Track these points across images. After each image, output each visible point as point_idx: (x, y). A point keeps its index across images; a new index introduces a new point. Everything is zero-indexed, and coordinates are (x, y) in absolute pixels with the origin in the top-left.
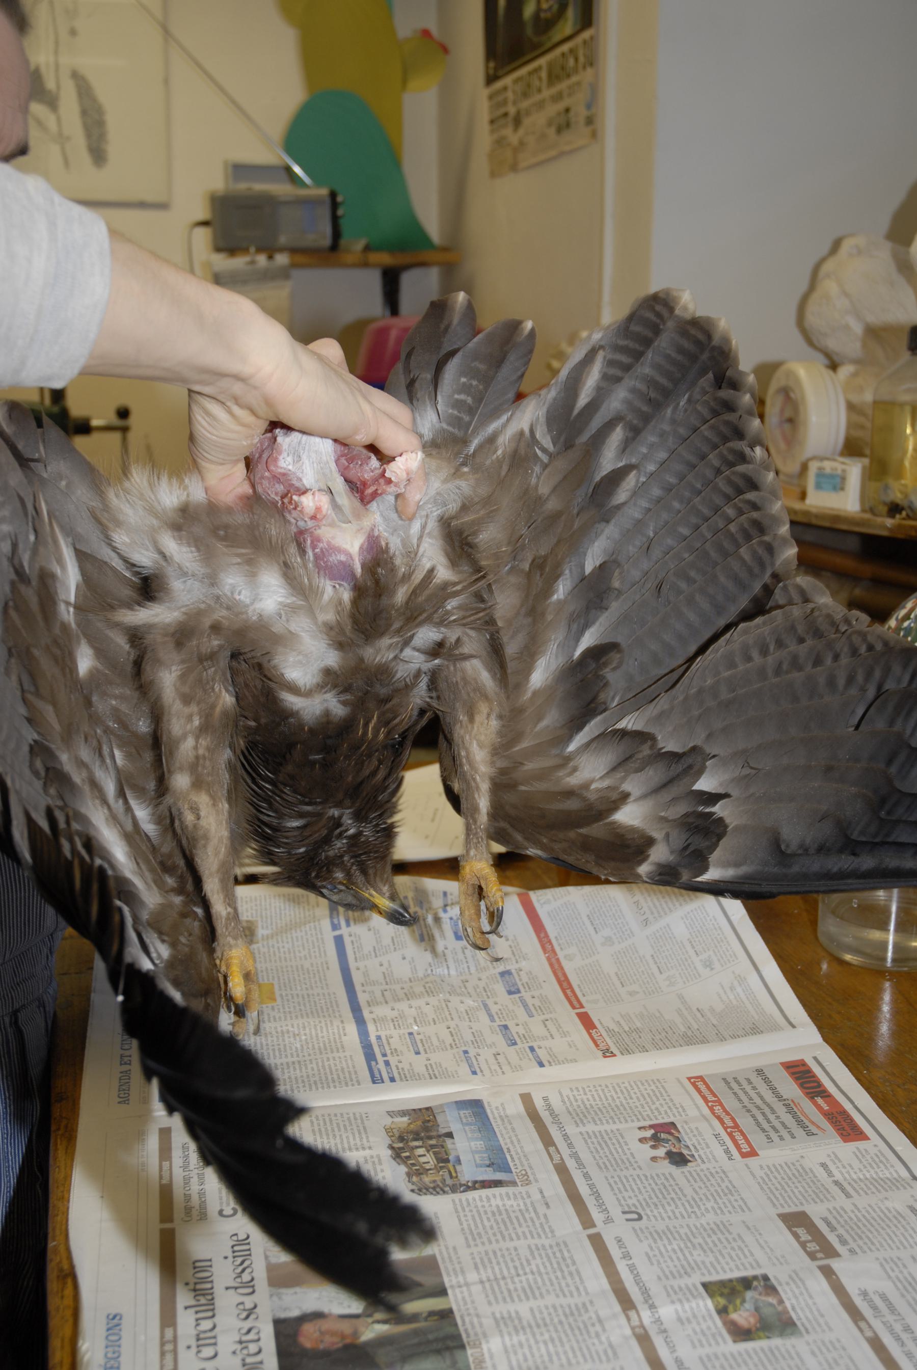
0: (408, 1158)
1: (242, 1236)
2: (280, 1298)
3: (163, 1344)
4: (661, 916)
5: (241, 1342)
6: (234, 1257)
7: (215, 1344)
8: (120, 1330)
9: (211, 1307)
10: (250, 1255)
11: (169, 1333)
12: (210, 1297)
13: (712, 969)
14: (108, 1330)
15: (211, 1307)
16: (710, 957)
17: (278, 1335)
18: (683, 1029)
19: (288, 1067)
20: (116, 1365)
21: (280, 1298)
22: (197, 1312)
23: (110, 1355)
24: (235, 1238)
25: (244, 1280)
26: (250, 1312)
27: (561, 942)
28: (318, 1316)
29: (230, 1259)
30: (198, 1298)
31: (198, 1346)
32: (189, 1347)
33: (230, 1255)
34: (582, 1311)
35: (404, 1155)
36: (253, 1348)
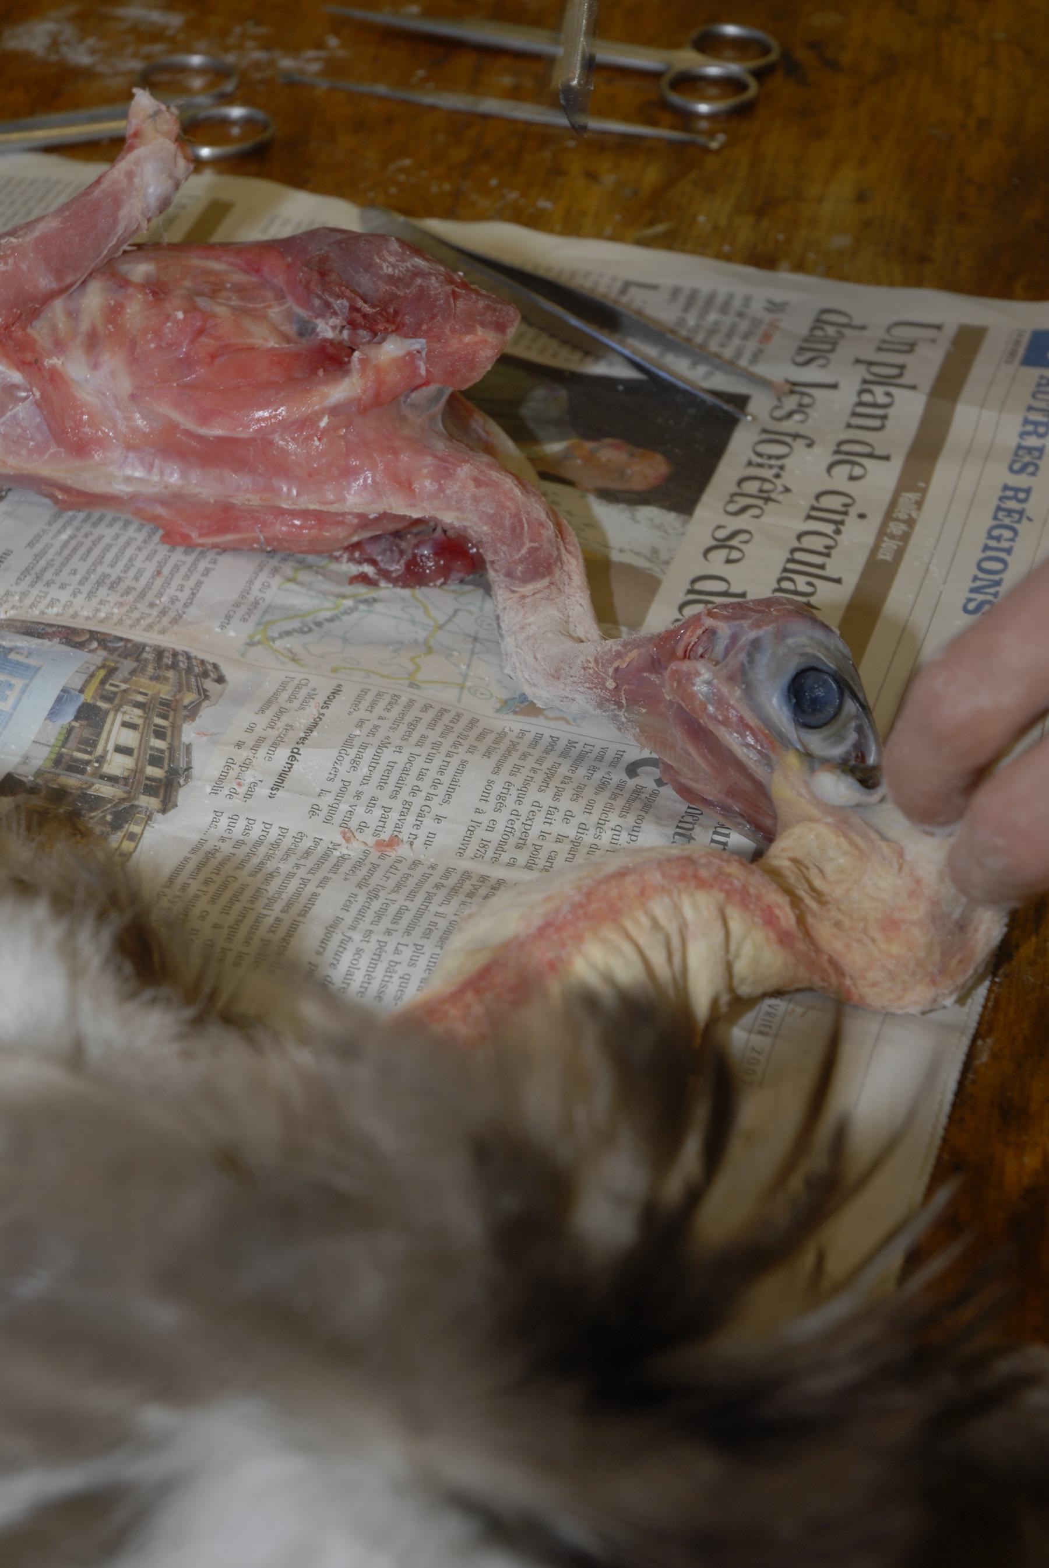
0: (155, 760)
3: (905, 537)
8: (975, 578)
11: (886, 554)
20: (1000, 515)
21: (655, 551)
22: (822, 567)
26: (722, 544)
30: (809, 589)
31: (846, 513)
32: (862, 516)
36: (752, 487)
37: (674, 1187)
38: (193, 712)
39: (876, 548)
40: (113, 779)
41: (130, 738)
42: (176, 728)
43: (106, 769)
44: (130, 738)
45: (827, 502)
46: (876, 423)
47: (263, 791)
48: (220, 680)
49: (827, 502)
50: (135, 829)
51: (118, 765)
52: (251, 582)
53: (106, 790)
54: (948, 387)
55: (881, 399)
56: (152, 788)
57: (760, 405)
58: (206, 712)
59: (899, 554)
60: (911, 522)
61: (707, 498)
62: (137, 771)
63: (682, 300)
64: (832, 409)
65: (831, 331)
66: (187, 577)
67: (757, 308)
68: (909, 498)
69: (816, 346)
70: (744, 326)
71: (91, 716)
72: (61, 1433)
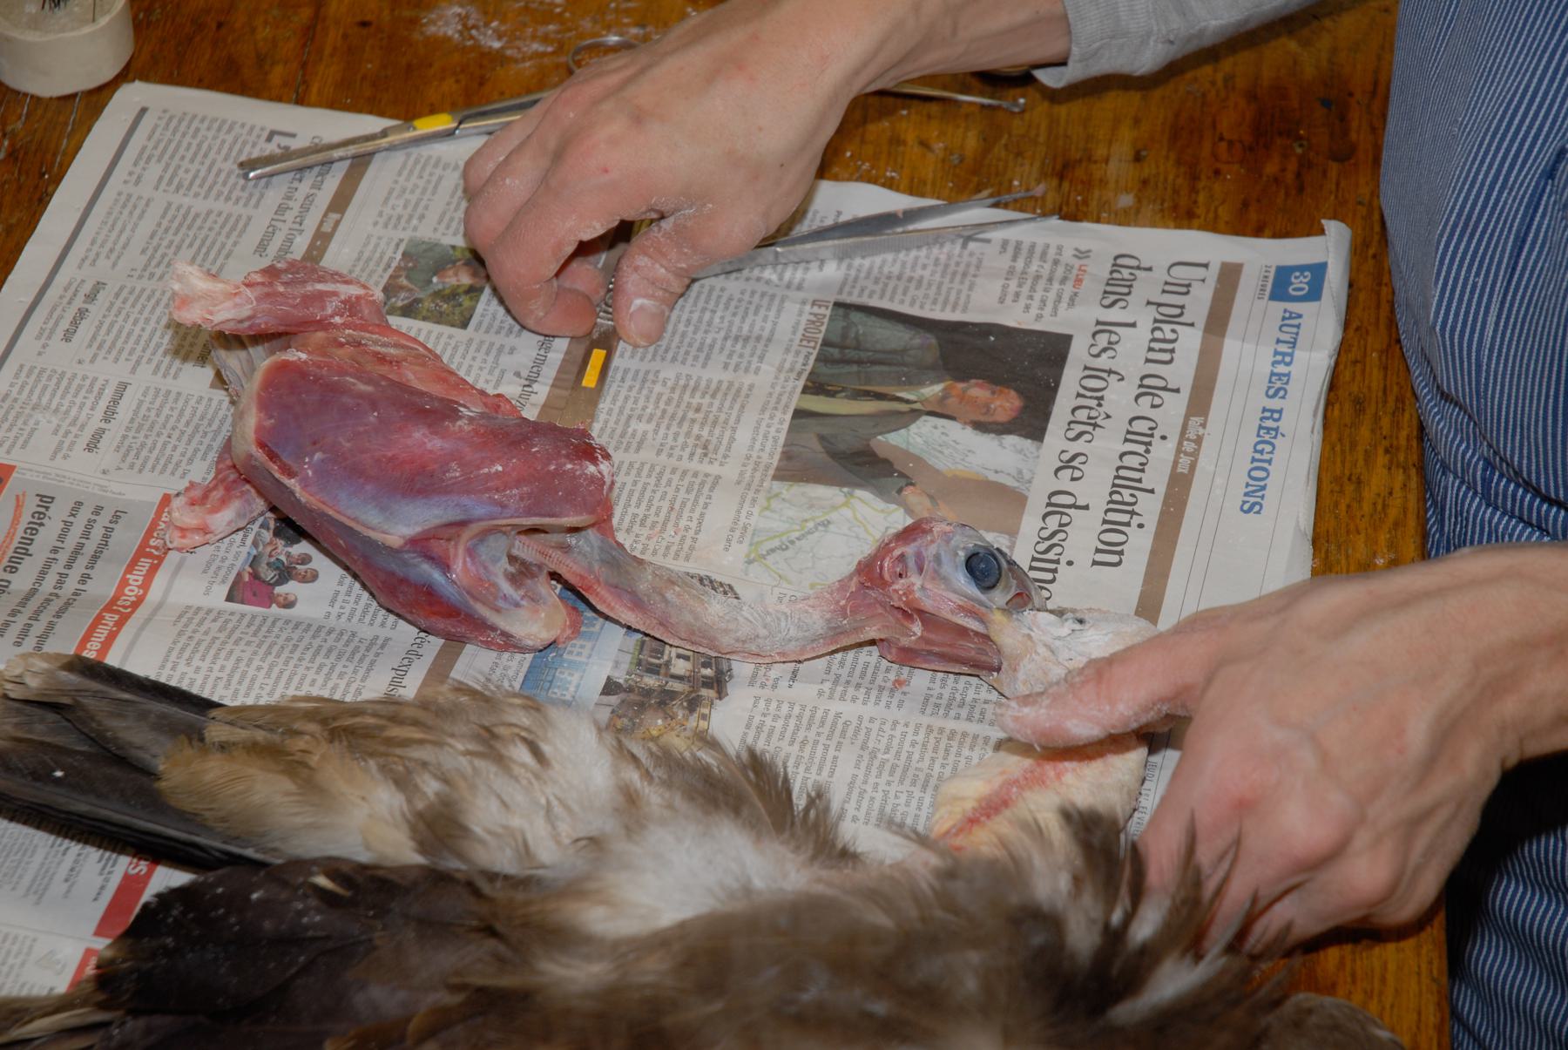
2: (1020, 472)
5: (1095, 425)
6: (1058, 562)
7: (1129, 432)
9: (1118, 482)
10: (1034, 559)
12: (1116, 497)
14: (1263, 488)
15: (1118, 482)
17: (1046, 416)
22: (1140, 481)
23: (1268, 448)
25: (1106, 335)
26: (1067, 465)
28: (981, 427)
29: (1063, 560)
32: (1164, 438)
33: (1062, 568)
34: (641, 375)
35: (708, 672)
36: (1082, 415)
37: (1117, 917)
39: (1176, 463)
40: (680, 678)
43: (673, 670)
46: (1166, 357)
50: (705, 711)
52: (739, 512)
53: (676, 686)
54: (1217, 323)
55: (1172, 336)
56: (708, 683)
57: (1078, 353)
59: (1193, 467)
60: (1199, 441)
63: (1010, 250)
65: (1126, 273)
66: (692, 511)
67: (1068, 255)
68: (1195, 421)
69: (1117, 288)
70: (1060, 271)
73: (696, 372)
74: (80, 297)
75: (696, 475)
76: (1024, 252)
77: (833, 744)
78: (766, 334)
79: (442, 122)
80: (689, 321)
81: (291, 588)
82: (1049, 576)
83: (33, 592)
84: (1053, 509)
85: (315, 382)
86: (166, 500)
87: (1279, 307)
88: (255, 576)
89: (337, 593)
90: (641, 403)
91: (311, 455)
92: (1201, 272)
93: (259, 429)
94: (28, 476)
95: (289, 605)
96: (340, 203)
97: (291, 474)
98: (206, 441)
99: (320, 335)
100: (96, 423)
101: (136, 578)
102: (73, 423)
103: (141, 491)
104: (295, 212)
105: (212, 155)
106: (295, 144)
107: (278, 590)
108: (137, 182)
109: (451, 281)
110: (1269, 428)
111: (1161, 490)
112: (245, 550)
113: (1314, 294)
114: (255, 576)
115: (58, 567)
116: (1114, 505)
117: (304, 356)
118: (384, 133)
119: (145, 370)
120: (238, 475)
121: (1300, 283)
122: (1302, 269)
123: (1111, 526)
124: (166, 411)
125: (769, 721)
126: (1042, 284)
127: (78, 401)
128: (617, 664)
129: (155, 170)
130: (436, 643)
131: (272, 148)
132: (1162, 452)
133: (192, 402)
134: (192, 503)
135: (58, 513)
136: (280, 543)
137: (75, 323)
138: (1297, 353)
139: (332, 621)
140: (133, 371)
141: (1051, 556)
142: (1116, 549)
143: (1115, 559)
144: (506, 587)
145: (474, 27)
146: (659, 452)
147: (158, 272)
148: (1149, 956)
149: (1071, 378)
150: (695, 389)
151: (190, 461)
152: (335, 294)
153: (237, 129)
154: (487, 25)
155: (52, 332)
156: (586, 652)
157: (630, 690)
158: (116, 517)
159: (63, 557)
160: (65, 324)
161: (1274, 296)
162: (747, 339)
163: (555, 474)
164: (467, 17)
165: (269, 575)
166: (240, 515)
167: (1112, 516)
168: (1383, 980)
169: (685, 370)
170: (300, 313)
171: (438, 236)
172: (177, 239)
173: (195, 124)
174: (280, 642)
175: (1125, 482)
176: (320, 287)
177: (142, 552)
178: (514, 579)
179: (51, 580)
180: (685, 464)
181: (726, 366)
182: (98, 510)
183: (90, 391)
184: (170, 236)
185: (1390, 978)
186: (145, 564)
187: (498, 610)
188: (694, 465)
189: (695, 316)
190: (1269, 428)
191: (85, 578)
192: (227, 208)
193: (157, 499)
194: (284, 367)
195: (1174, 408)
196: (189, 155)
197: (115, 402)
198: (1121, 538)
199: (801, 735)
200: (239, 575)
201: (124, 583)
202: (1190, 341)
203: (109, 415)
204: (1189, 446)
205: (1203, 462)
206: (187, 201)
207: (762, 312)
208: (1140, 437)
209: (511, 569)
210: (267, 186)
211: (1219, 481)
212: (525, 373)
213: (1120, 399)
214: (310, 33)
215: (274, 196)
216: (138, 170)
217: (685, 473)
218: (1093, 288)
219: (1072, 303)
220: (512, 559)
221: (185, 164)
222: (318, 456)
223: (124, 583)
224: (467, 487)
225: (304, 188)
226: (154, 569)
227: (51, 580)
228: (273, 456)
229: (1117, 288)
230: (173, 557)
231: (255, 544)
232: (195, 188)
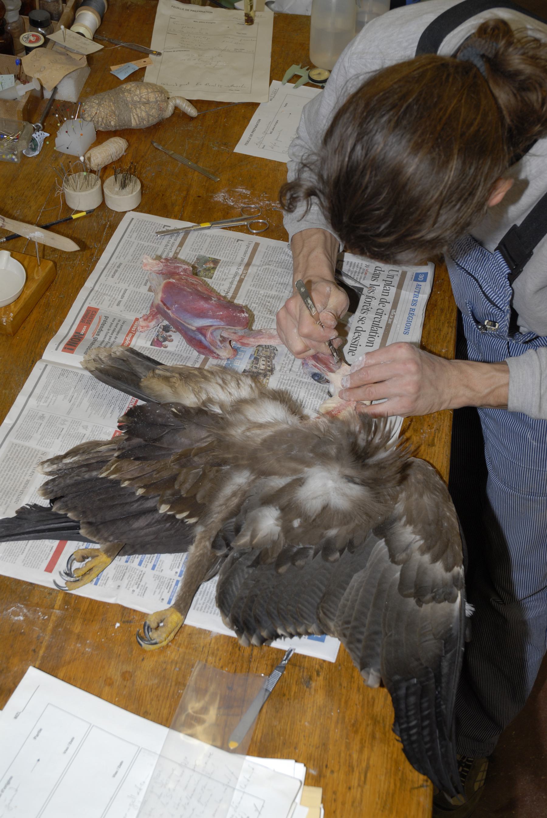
0: (269, 366)
1: (351, 353)
4: (36, 450)
13: (43, 415)
16: (38, 420)
18: (90, 392)
19: (297, 382)
24: (354, 354)
26: (361, 320)
27: (49, 551)
33: (358, 347)
35: (270, 368)
36: (365, 308)
37: (370, 438)
38: (274, 358)
39: (388, 321)
40: (262, 370)
41: (264, 363)
42: (271, 361)
44: (264, 363)
45: (379, 311)
46: (387, 294)
47: (288, 372)
48: (277, 350)
49: (379, 311)
51: (262, 367)
53: (261, 371)
54: (400, 286)
55: (388, 289)
56: (269, 371)
57: (365, 291)
58: (276, 358)
59: (392, 322)
60: (394, 316)
61: (357, 310)
62: (266, 368)
63: (349, 264)
64: (379, 290)
65: (378, 272)
67: (364, 266)
68: (393, 310)
69: (375, 276)
70: (361, 270)
71: (257, 359)
72: (295, 471)
73: (269, 292)
74: (116, 267)
75: (268, 318)
76: (353, 265)
77: (299, 387)
78: (287, 283)
79: (207, 225)
80: (268, 278)
81: (166, 343)
82: (355, 349)
83: (103, 341)
84: (357, 331)
85: (177, 287)
86: (137, 320)
87: (415, 283)
88: (158, 339)
89: (178, 345)
90: (255, 299)
91: (175, 305)
92: (397, 273)
93: (162, 298)
94: (102, 311)
95: (166, 347)
96: (181, 245)
97: (169, 309)
98: (146, 305)
99: (178, 276)
100: (119, 299)
101: (128, 338)
102: (114, 299)
103: (130, 317)
104: (170, 247)
105: (149, 231)
106: (169, 229)
107: (163, 343)
108: (131, 238)
109: (208, 266)
110: (412, 313)
111: (384, 327)
112: (155, 333)
113: (425, 280)
114: (158, 339)
115: (109, 334)
116: (372, 331)
117: (174, 281)
118: (193, 227)
119: (132, 286)
120: (157, 311)
121: (421, 277)
122: (422, 274)
123: (371, 336)
124: (136, 297)
125: (284, 381)
126: (357, 273)
127: (115, 293)
128: (247, 366)
129: (135, 234)
130: (203, 357)
131: (164, 229)
132: (385, 318)
133: (143, 295)
134: (144, 320)
135: (109, 321)
136: (164, 332)
137: (115, 273)
138: (420, 295)
139: (176, 352)
140: (129, 286)
141: (355, 343)
142: (372, 342)
143: (371, 345)
144: (219, 343)
145: (227, 199)
146: (259, 312)
147: (135, 261)
148: (377, 449)
149: (363, 299)
150: (268, 296)
151: (142, 310)
152: (181, 267)
153: (156, 225)
154: (230, 199)
155: (109, 275)
156: (239, 363)
157: (250, 372)
158: (124, 323)
159: (111, 332)
160: (112, 273)
161: (414, 280)
162: (282, 284)
163: (234, 316)
164: (225, 196)
165: (161, 339)
166: (156, 323)
167: (371, 334)
168: (434, 455)
169: (266, 291)
170: (173, 270)
171: (205, 255)
172: (140, 252)
173: (145, 223)
174: (164, 357)
175: (375, 325)
176: (178, 265)
177: (130, 331)
178: (221, 342)
179: (108, 338)
180: (265, 315)
181: (276, 291)
182: (119, 321)
183: (118, 291)
184: (138, 252)
185: (436, 454)
186: (131, 335)
187: (217, 349)
188: (268, 316)
189: (269, 277)
190: (412, 313)
191: (116, 338)
192: (153, 245)
193: (134, 319)
194: (170, 282)
195: (388, 307)
196: (144, 231)
197: (124, 294)
198: (373, 339)
199: (292, 384)
200: (154, 339)
201: (125, 339)
202: (393, 290)
203: (122, 297)
204: (391, 317)
205: (395, 321)
206: (143, 243)
207: (286, 277)
208: (380, 314)
209: (221, 339)
210: (163, 239)
211: (398, 326)
212: (226, 291)
213: (375, 304)
214: (185, 198)
215: (164, 242)
216: (131, 234)
217: (265, 318)
218: (369, 276)
219: (364, 279)
220: (221, 336)
221: (143, 233)
222: (176, 306)
223: (125, 339)
224: (213, 317)
225: (172, 240)
226: (133, 336)
227: (108, 338)
228: (165, 305)
229: (375, 276)
230: (137, 333)
231: (158, 332)
232: (145, 239)
